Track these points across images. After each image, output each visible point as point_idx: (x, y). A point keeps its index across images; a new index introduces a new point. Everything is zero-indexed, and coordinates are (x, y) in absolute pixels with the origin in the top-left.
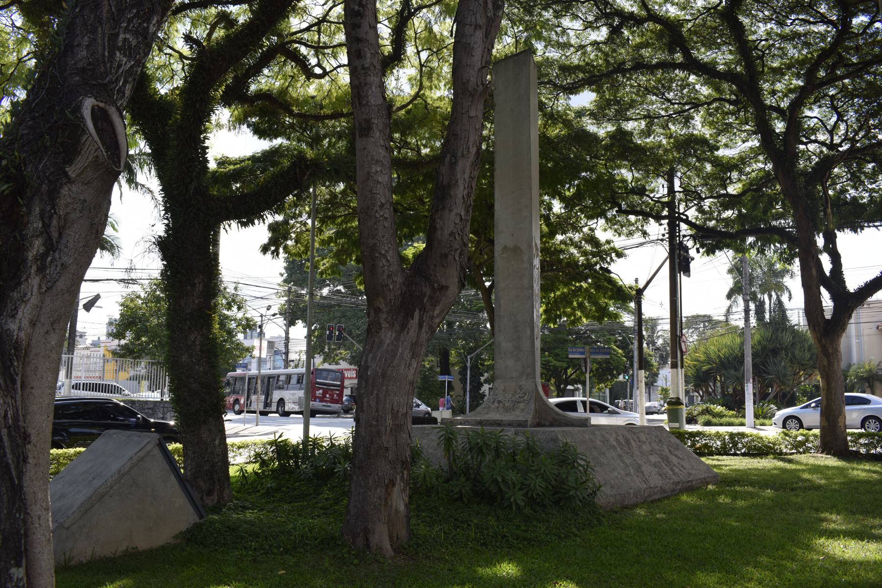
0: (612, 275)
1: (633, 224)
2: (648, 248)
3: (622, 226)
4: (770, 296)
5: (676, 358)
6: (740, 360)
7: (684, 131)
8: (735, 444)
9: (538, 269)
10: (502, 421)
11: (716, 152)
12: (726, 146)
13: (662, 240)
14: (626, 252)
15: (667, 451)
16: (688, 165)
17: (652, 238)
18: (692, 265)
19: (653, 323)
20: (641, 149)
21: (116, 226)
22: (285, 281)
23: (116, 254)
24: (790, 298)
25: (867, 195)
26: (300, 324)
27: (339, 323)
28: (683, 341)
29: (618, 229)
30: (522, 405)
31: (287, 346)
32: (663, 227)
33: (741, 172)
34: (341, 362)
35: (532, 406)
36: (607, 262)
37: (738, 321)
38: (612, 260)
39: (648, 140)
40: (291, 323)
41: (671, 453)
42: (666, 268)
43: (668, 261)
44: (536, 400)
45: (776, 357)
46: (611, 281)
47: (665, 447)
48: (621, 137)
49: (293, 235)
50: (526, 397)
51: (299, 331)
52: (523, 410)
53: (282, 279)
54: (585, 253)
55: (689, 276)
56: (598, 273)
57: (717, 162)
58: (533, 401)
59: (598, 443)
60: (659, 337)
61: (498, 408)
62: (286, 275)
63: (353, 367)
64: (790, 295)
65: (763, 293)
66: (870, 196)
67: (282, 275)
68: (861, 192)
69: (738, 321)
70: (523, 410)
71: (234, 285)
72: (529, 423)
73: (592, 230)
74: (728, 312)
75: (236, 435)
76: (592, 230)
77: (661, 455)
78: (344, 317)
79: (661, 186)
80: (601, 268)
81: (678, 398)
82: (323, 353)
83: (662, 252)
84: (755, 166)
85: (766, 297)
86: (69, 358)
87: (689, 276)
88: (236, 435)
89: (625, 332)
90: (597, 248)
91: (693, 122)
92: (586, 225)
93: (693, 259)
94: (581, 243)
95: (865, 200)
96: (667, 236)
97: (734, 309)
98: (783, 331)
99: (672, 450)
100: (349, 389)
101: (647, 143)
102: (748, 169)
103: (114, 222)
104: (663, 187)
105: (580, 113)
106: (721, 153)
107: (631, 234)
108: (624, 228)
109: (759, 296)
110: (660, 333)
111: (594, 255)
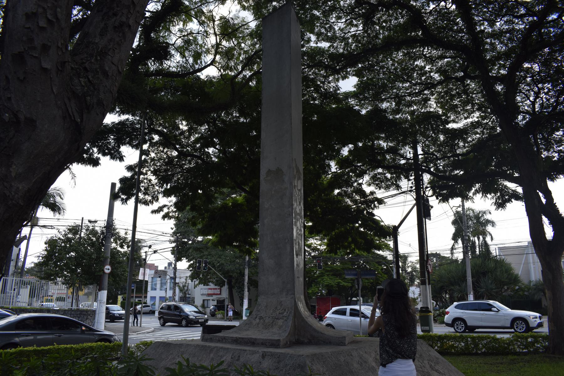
0: (376, 217)
1: (389, 180)
2: (401, 198)
3: (382, 182)
4: (479, 239)
5: (425, 277)
6: (464, 278)
7: (423, 110)
8: (476, 345)
9: (300, 190)
10: (256, 339)
11: (447, 126)
12: (454, 121)
13: (411, 191)
14: (385, 200)
15: (428, 366)
16: (427, 137)
17: (403, 190)
18: (432, 211)
19: (405, 258)
20: (394, 122)
21: (62, 196)
22: (174, 233)
23: (62, 213)
24: (492, 239)
25: (556, 155)
26: (184, 260)
27: (207, 259)
28: (429, 264)
29: (379, 184)
30: (280, 322)
31: (175, 274)
32: (410, 182)
33: (465, 141)
34: (210, 284)
35: (290, 323)
36: (371, 207)
37: (459, 255)
38: (375, 206)
39: (398, 117)
40: (178, 259)
41: (432, 369)
42: (414, 214)
43: (415, 208)
44: (295, 316)
45: (485, 276)
46: (377, 223)
47: (426, 362)
48: (377, 113)
49: (143, 189)
50: (285, 313)
51: (183, 265)
52: (280, 327)
53: (173, 231)
54: (355, 202)
55: (430, 219)
56: (366, 216)
57: (447, 132)
58: (291, 318)
59: (355, 365)
60: (409, 267)
61: (258, 324)
62: (175, 229)
63: (217, 287)
64: (492, 237)
65: (474, 237)
66: (559, 155)
67: (172, 229)
68: (552, 153)
69: (459, 255)
70: (280, 327)
71: (124, 231)
72: (282, 343)
73: (360, 184)
74: (453, 249)
75: (121, 335)
76: (360, 184)
77: (423, 372)
78: (210, 255)
79: (408, 152)
80: (368, 212)
81: (428, 308)
82: (199, 278)
83: (410, 199)
84: (474, 137)
85: (476, 238)
86: (20, 280)
87: (430, 219)
88: (121, 335)
89: (387, 263)
90: (364, 198)
91: (430, 102)
92: (356, 181)
93: (432, 207)
94: (353, 195)
95: (555, 159)
96: (414, 188)
97: (456, 246)
98: (488, 260)
99: (433, 365)
100: (216, 301)
101: (397, 119)
102: (469, 139)
103: (61, 194)
104: (410, 153)
105: (348, 95)
106: (451, 126)
107: (388, 187)
108: (383, 184)
109: (471, 239)
110: (409, 265)
111: (362, 203)
